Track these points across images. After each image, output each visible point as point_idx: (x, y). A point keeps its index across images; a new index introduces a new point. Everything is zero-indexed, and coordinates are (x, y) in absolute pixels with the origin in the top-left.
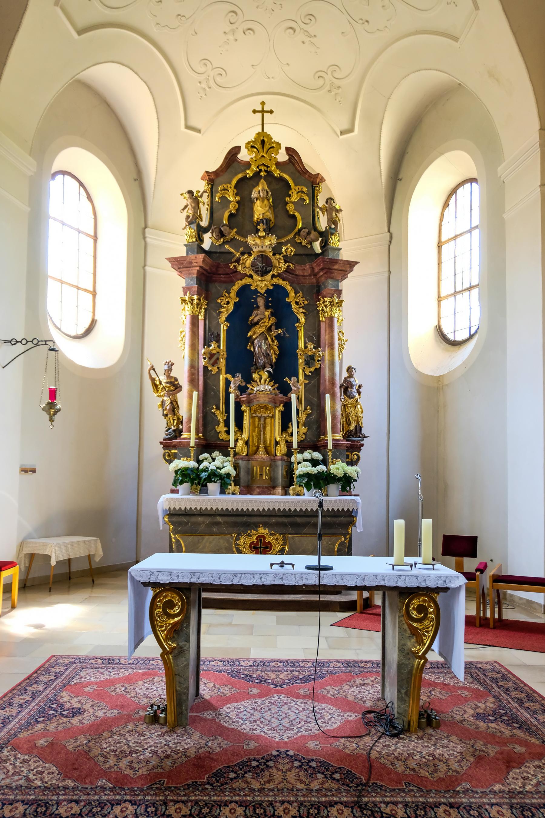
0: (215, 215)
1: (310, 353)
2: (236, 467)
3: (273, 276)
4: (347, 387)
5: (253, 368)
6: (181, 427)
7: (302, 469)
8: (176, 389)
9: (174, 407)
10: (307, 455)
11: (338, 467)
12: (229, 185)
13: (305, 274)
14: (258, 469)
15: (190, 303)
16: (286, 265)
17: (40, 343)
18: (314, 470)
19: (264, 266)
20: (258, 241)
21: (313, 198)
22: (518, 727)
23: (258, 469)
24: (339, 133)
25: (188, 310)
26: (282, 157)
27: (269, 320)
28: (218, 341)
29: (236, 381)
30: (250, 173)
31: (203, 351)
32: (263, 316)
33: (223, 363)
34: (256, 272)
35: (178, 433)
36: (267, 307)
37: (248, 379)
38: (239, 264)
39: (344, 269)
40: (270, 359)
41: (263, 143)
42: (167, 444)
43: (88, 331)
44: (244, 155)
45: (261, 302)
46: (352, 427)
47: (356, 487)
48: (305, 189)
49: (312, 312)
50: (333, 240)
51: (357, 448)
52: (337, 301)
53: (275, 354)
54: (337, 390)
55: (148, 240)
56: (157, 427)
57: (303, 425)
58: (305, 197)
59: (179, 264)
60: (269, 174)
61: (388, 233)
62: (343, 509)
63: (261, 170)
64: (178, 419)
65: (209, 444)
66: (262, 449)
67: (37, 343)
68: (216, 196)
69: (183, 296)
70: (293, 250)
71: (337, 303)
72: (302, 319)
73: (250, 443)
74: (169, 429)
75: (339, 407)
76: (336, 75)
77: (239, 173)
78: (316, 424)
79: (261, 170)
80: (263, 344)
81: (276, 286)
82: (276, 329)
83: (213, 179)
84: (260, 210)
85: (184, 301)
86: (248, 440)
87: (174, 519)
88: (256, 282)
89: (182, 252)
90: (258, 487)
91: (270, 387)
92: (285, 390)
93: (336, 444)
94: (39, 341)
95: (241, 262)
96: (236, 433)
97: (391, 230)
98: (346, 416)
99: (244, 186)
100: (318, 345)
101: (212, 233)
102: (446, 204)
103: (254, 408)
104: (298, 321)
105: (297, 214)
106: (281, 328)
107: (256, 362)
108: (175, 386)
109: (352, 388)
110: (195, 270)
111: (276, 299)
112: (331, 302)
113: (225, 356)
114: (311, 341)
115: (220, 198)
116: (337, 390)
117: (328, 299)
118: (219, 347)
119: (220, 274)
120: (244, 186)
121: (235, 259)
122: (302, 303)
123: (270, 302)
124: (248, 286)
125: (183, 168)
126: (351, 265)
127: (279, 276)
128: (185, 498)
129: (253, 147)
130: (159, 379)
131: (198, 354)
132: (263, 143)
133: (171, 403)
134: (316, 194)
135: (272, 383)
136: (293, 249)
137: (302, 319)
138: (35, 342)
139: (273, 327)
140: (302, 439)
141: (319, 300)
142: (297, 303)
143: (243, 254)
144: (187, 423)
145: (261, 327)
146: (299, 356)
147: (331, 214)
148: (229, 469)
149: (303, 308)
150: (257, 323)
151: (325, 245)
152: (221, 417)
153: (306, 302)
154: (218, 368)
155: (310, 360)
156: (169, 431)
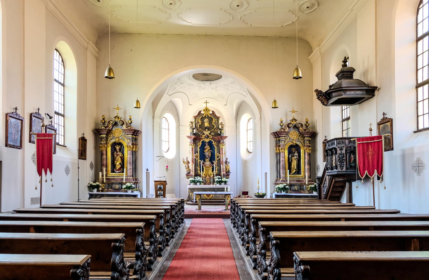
2: (203, 179)
4: (226, 162)
7: (216, 180)
9: (188, 167)
10: (218, 177)
11: (224, 179)
18: (219, 180)
19: (207, 137)
21: (218, 121)
25: (191, 147)
26: (211, 112)
29: (202, 162)
30: (204, 116)
32: (207, 147)
33: (199, 158)
35: (189, 173)
37: (205, 161)
41: (206, 110)
42: (187, 175)
43: (168, 150)
44: (202, 112)
45: (207, 144)
47: (228, 183)
49: (218, 146)
50: (222, 131)
54: (224, 163)
56: (184, 171)
59: (189, 137)
60: (208, 116)
65: (196, 175)
67: (161, 157)
75: (224, 167)
78: (219, 170)
80: (207, 153)
83: (195, 118)
84: (206, 124)
89: (189, 135)
92: (213, 163)
93: (224, 175)
98: (226, 168)
100: (220, 154)
102: (248, 122)
108: (188, 163)
111: (210, 143)
116: (224, 163)
124: (204, 141)
125: (188, 116)
126: (226, 137)
128: (192, 186)
132: (206, 110)
136: (219, 99)
148: (201, 180)
151: (221, 132)
155: (218, 157)
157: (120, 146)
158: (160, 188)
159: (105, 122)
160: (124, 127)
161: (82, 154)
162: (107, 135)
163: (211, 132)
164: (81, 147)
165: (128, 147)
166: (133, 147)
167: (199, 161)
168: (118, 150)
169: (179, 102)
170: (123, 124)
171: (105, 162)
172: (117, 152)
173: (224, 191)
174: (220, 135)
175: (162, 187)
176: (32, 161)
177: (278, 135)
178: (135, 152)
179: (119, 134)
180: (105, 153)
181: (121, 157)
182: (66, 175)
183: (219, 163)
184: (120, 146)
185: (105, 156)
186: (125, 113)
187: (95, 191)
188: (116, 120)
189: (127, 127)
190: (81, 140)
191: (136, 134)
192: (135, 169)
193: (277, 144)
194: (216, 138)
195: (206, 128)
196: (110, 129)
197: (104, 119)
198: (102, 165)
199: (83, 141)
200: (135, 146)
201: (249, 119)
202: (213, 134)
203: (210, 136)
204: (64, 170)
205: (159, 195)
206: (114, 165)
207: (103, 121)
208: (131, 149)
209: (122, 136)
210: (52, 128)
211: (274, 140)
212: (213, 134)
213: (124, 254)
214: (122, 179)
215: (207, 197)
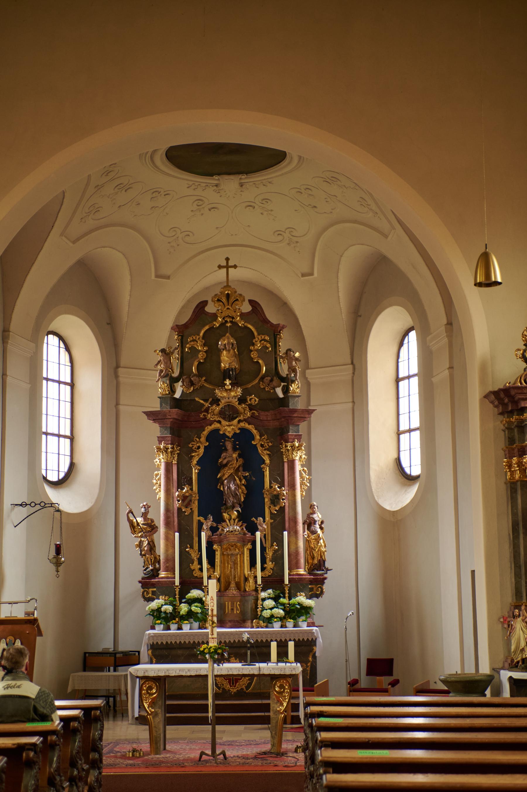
0: (185, 364)
1: (275, 493)
3: (239, 421)
4: (309, 523)
5: (223, 508)
6: (157, 566)
8: (152, 530)
9: (152, 547)
12: (198, 337)
13: (269, 419)
14: (230, 604)
15: (165, 451)
16: (251, 412)
17: (47, 505)
19: (229, 413)
20: (225, 394)
21: (275, 345)
22: (160, 608)
23: (230, 604)
24: (300, 275)
27: (237, 461)
28: (190, 484)
29: (208, 524)
31: (177, 493)
32: (232, 457)
33: (195, 506)
34: (224, 419)
35: (155, 573)
36: (235, 449)
37: (219, 519)
38: (208, 413)
39: (303, 416)
40: (239, 498)
42: (145, 583)
44: (211, 308)
45: (229, 445)
46: (316, 561)
48: (267, 338)
51: (321, 581)
52: (297, 445)
53: (243, 493)
55: (121, 379)
56: (133, 568)
57: (270, 561)
58: (268, 345)
59: (152, 415)
61: (351, 366)
62: (303, 639)
63: (226, 322)
64: (155, 558)
66: (233, 585)
68: (186, 347)
69: (159, 445)
70: (257, 400)
71: (298, 447)
72: (268, 461)
73: (222, 580)
74: (147, 568)
76: (293, 234)
77: (207, 324)
79: (226, 322)
80: (232, 486)
81: (242, 430)
82: (243, 471)
83: (182, 331)
84: (226, 360)
85: (159, 449)
86: (220, 577)
87: (157, 653)
88: (224, 427)
89: (156, 406)
90: (230, 621)
91: (238, 528)
94: (45, 504)
95: (210, 411)
96: (208, 570)
97: (354, 362)
99: (211, 339)
101: (183, 382)
102: (401, 344)
103: (225, 547)
104: (263, 462)
105: (260, 361)
106: (248, 471)
107: (225, 501)
109: (315, 523)
110: (168, 422)
111: (243, 439)
112: (292, 447)
113: (198, 498)
114: (277, 482)
115: (189, 348)
117: (289, 444)
118: (191, 489)
119: (191, 422)
120: (211, 339)
121: (205, 408)
122: (266, 445)
123: (238, 445)
124: (217, 430)
125: (154, 327)
127: (245, 420)
129: (219, 300)
130: (137, 520)
131: (173, 498)
133: (149, 544)
134: (278, 340)
135: (240, 523)
137: (268, 461)
138: (42, 504)
139: (241, 469)
140: (270, 574)
141: (281, 444)
142: (262, 446)
143: (212, 404)
144: (164, 563)
145: (229, 469)
146: (265, 496)
147: (291, 363)
149: (268, 449)
150: (226, 465)
151: (286, 390)
152: (194, 556)
153: (270, 444)
154: (191, 509)
155: (276, 499)
156: (147, 570)
163: (246, 392)
167: (196, 518)
169: (117, 258)
173: (266, 658)
174: (284, 402)
177: (516, 402)
183: (282, 522)
193: (511, 441)
194: (267, 416)
195: (226, 374)
201: (406, 333)
202: (254, 400)
203: (240, 408)
211: (498, 424)
212: (254, 400)
213: (176, 585)
215: (227, 687)
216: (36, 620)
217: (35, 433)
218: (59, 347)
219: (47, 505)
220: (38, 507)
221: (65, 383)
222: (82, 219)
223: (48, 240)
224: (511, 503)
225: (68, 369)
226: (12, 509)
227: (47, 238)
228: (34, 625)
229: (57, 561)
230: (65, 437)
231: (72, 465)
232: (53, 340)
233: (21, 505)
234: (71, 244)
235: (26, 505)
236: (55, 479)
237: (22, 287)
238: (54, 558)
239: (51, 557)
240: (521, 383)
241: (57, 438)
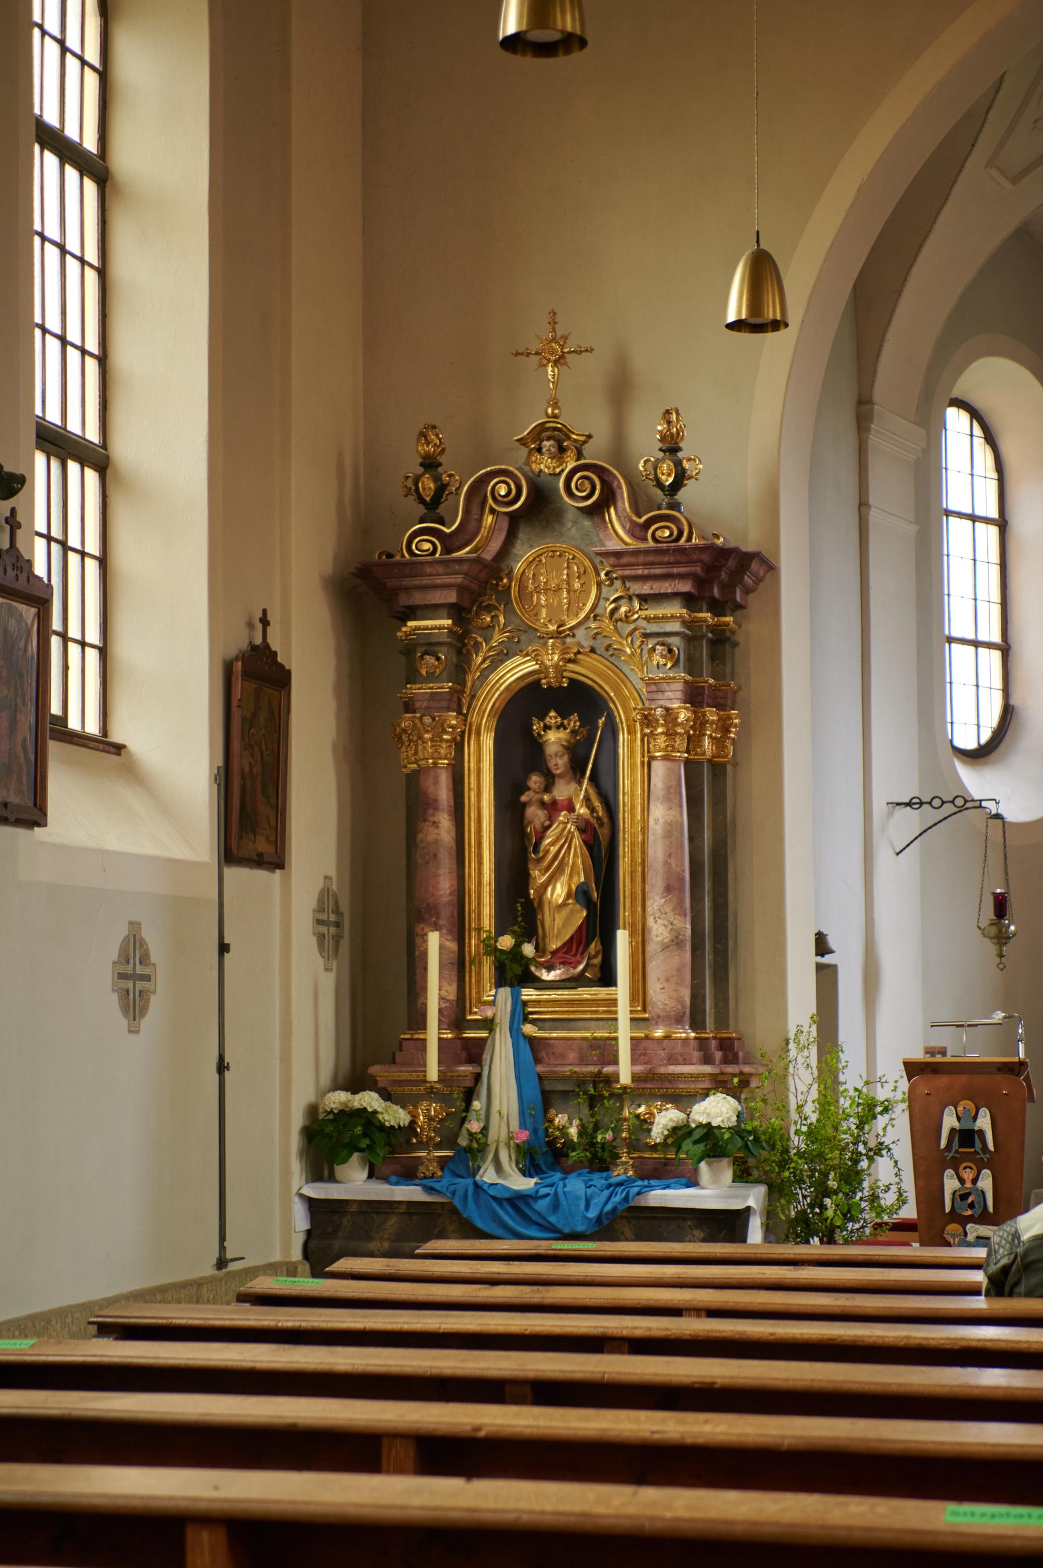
17: (968, 805)
94: (966, 801)
138: (959, 802)
157: (574, 722)
158: (967, 1137)
159: (441, 489)
160: (617, 532)
161: (250, 819)
162: (458, 612)
164: (248, 746)
165: (648, 720)
166: (699, 724)
168: (559, 763)
170: (609, 497)
171: (445, 886)
172: (550, 780)
175: (984, 1122)
176: (114, 999)
178: (718, 769)
179: (579, 609)
180: (444, 793)
181: (585, 828)
182: (123, 1022)
184: (574, 722)
185: (445, 821)
186: (620, 390)
187: (354, 1183)
188: (544, 464)
189: (638, 531)
190: (246, 674)
191: (728, 587)
192: (717, 943)
196: (489, 555)
197: (430, 464)
198: (419, 915)
199: (252, 689)
200: (712, 715)
204: (107, 976)
205: (954, 1216)
206: (519, 907)
207: (428, 485)
208: (681, 743)
209: (594, 614)
210: (21, 584)
214: (607, 1050)
216: (1022, 1064)
217: (931, 639)
218: (972, 436)
219: (968, 805)
220: (949, 809)
221: (987, 521)
222: (1036, 120)
223: (960, 179)
224: (726, 817)
225: (993, 486)
226: (890, 814)
227: (958, 175)
228: (1018, 1075)
229: (1000, 931)
230: (990, 645)
231: (1008, 712)
232: (956, 420)
233: (909, 804)
234: (1007, 185)
235: (921, 803)
236: (971, 744)
237: (900, 295)
238: (992, 924)
239: (984, 923)
240: (403, 556)
241: (972, 649)
